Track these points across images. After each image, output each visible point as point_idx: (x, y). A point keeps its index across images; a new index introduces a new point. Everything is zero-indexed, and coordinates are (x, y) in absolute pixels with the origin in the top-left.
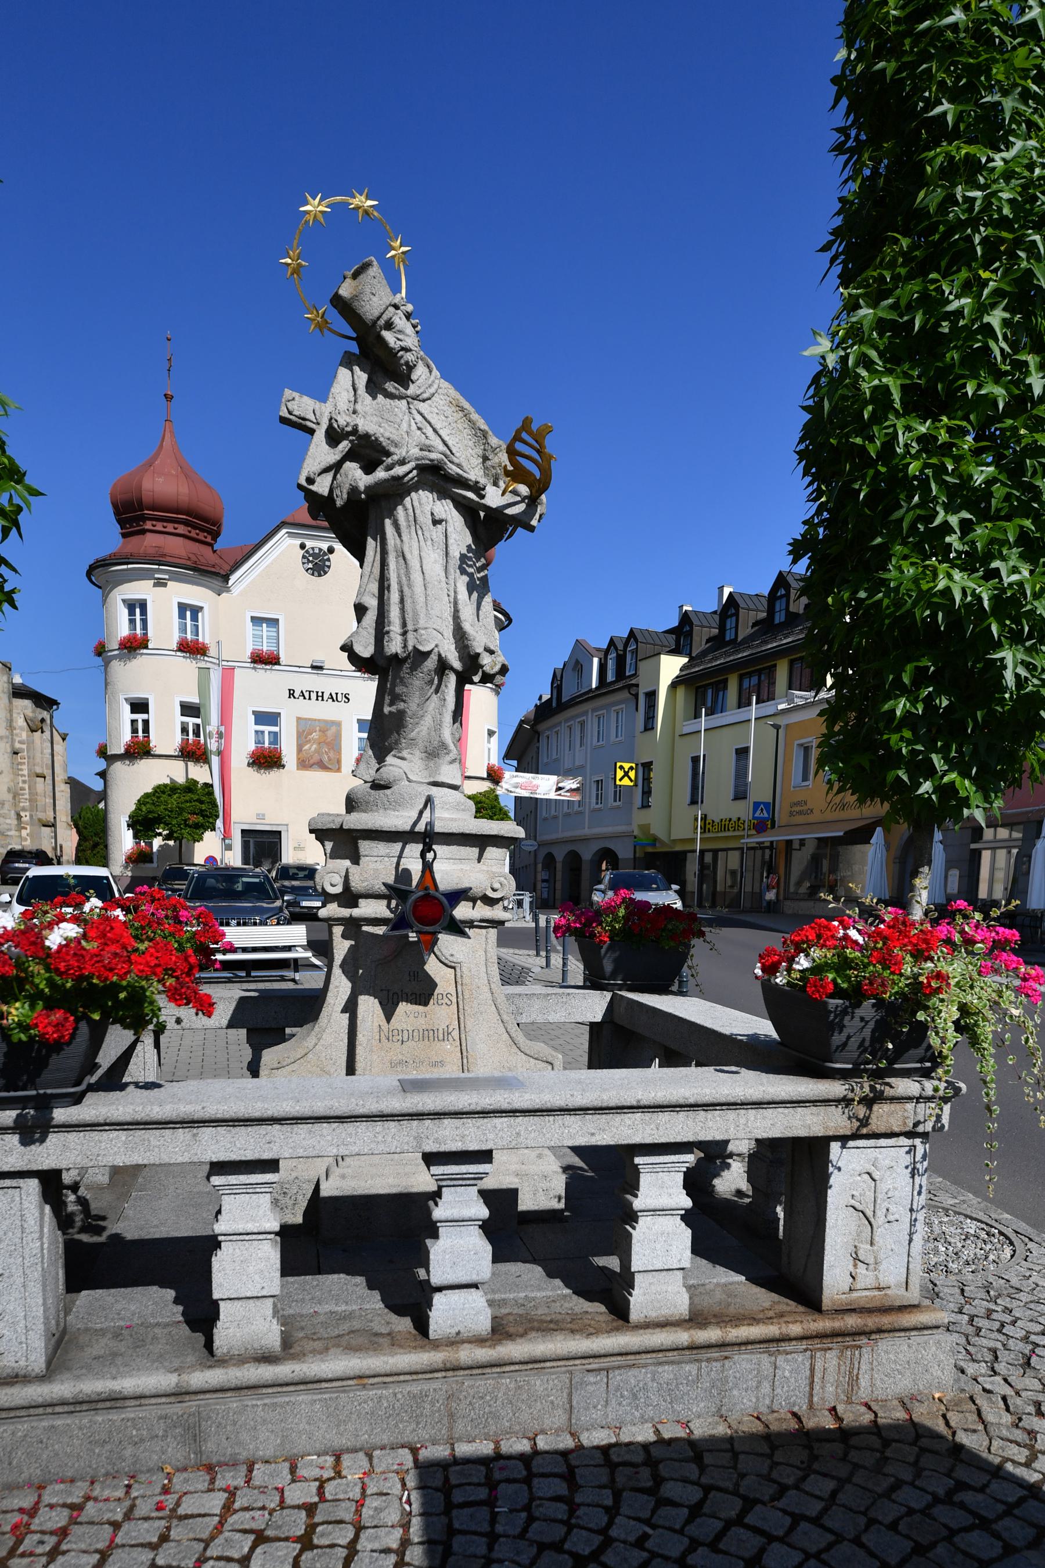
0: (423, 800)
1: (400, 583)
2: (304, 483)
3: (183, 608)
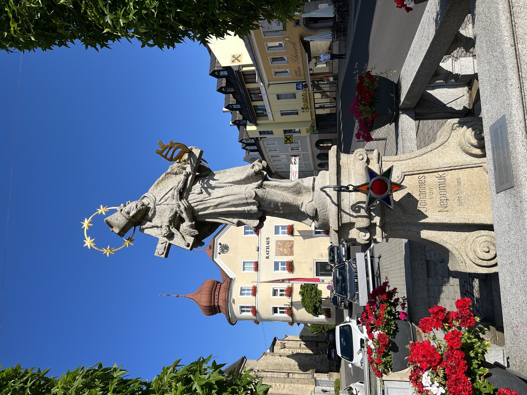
0: (322, 193)
1: (227, 207)
2: (189, 248)
3: (241, 294)
